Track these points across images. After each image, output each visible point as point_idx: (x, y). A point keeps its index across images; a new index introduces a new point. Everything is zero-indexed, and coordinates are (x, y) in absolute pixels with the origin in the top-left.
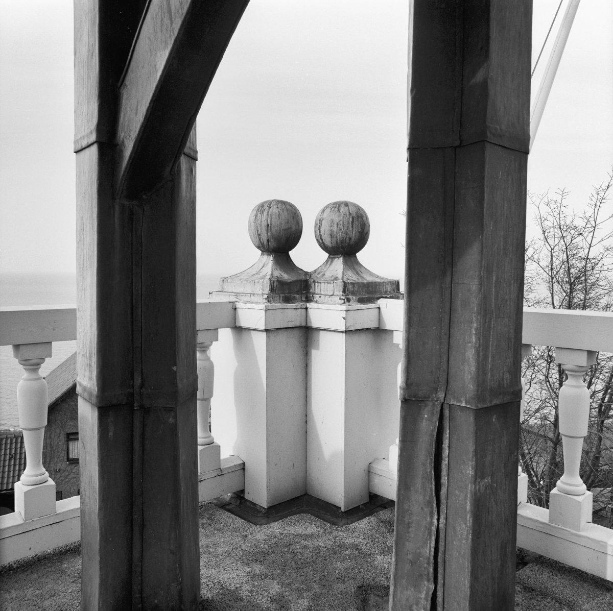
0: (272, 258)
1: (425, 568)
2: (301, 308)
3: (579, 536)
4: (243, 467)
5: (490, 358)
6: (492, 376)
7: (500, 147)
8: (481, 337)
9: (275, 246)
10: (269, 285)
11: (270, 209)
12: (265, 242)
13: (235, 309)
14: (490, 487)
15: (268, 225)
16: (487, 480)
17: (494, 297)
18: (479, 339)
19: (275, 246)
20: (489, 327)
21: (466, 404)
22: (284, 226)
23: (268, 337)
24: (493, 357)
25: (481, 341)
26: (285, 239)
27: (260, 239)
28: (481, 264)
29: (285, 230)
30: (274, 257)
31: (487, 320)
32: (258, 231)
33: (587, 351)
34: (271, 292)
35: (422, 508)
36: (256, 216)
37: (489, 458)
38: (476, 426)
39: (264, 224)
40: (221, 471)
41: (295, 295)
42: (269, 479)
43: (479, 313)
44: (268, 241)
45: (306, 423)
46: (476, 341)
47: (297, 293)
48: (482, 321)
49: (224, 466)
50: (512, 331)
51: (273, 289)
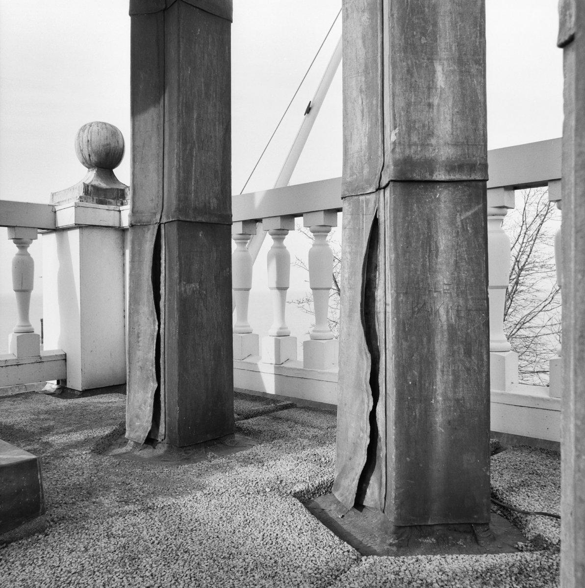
0: (94, 172)
1: (150, 370)
2: (114, 210)
3: (323, 373)
4: (64, 358)
5: (193, 181)
6: (196, 196)
7: (198, 9)
8: (181, 160)
9: (96, 160)
10: (83, 188)
11: (91, 127)
12: (87, 157)
13: (55, 212)
14: (198, 292)
15: (88, 141)
16: (195, 286)
17: (195, 131)
18: (179, 162)
19: (96, 160)
20: (191, 154)
21: (172, 218)
22: (103, 142)
23: (81, 234)
24: (197, 181)
25: (181, 164)
26: (104, 153)
27: (82, 154)
28: (179, 100)
29: (104, 146)
30: (97, 171)
31: (188, 148)
32: (80, 147)
33: (324, 211)
34: (85, 194)
35: (148, 319)
36: (79, 134)
37: (196, 267)
38: (178, 234)
39: (85, 140)
40: (41, 358)
41: (110, 200)
42: (83, 365)
43: (178, 140)
44: (89, 156)
45: (125, 318)
46: (177, 163)
47: (114, 199)
48: (181, 147)
49: (42, 355)
50: (218, 164)
51: (88, 193)
